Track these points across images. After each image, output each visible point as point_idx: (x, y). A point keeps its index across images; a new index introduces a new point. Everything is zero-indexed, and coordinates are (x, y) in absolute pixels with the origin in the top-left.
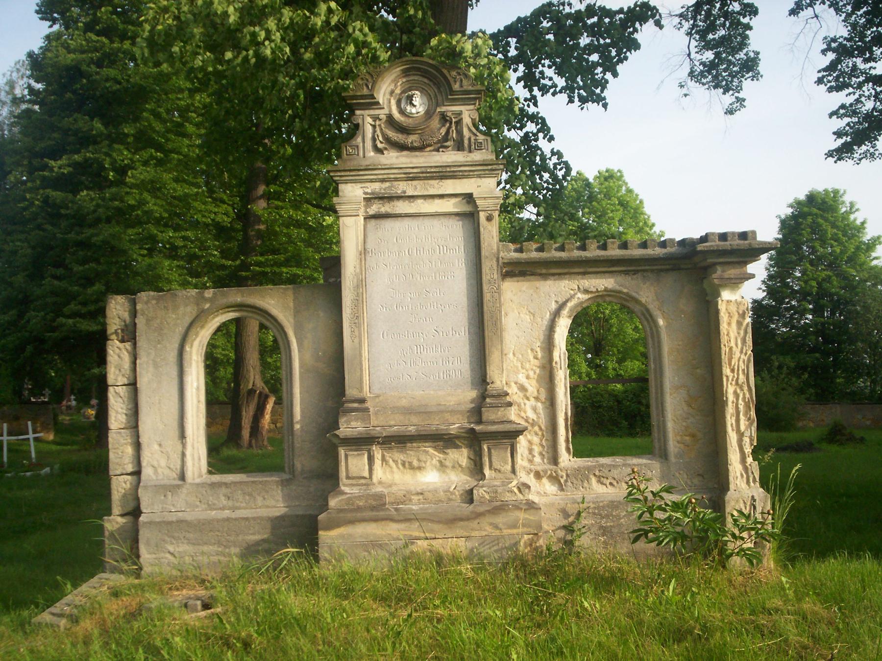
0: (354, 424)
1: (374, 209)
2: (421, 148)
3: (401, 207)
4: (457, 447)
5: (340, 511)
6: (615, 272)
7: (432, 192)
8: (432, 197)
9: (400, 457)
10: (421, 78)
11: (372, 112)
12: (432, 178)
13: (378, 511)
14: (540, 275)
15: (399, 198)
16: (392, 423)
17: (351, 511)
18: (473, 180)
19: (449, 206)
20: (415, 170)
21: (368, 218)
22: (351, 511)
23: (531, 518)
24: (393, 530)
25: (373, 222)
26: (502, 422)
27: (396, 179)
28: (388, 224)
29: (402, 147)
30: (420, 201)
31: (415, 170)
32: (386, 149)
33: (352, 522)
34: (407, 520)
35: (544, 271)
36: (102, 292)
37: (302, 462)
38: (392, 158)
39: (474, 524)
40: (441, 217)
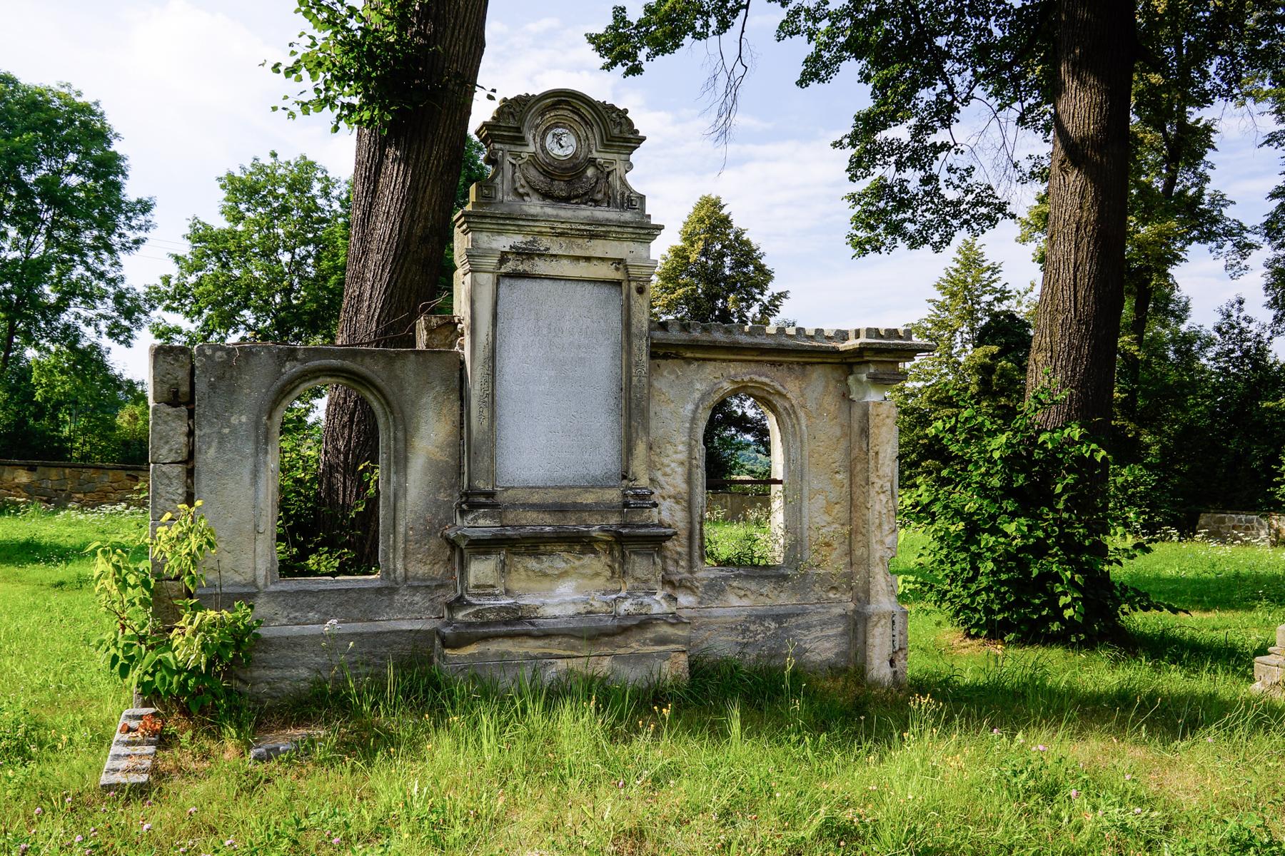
0: (481, 522)
1: (509, 267)
2: (567, 200)
3: (542, 267)
4: (595, 552)
5: (469, 625)
6: (750, 361)
7: (578, 253)
8: (578, 258)
9: (532, 563)
10: (571, 115)
11: (513, 148)
12: (582, 236)
13: (513, 625)
14: (684, 358)
15: (540, 255)
16: (524, 522)
17: (483, 625)
18: (625, 244)
19: (607, 272)
20: (564, 226)
21: (500, 278)
22: (483, 625)
23: (680, 633)
24: (532, 647)
25: (507, 281)
26: (646, 526)
27: (540, 233)
28: (525, 284)
29: (546, 195)
30: (565, 262)
31: (564, 226)
32: (528, 195)
33: (486, 638)
34: (547, 635)
35: (689, 355)
36: (77, 341)
37: (784, 600)
38: (534, 206)
39: (618, 639)
40: (586, 284)
